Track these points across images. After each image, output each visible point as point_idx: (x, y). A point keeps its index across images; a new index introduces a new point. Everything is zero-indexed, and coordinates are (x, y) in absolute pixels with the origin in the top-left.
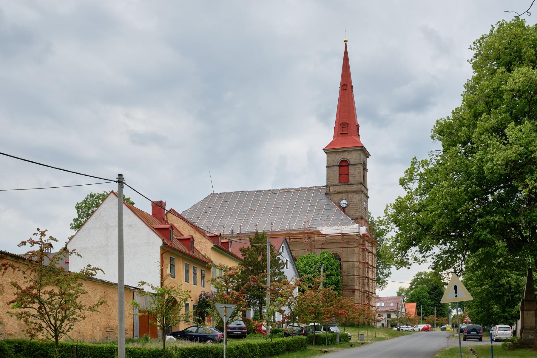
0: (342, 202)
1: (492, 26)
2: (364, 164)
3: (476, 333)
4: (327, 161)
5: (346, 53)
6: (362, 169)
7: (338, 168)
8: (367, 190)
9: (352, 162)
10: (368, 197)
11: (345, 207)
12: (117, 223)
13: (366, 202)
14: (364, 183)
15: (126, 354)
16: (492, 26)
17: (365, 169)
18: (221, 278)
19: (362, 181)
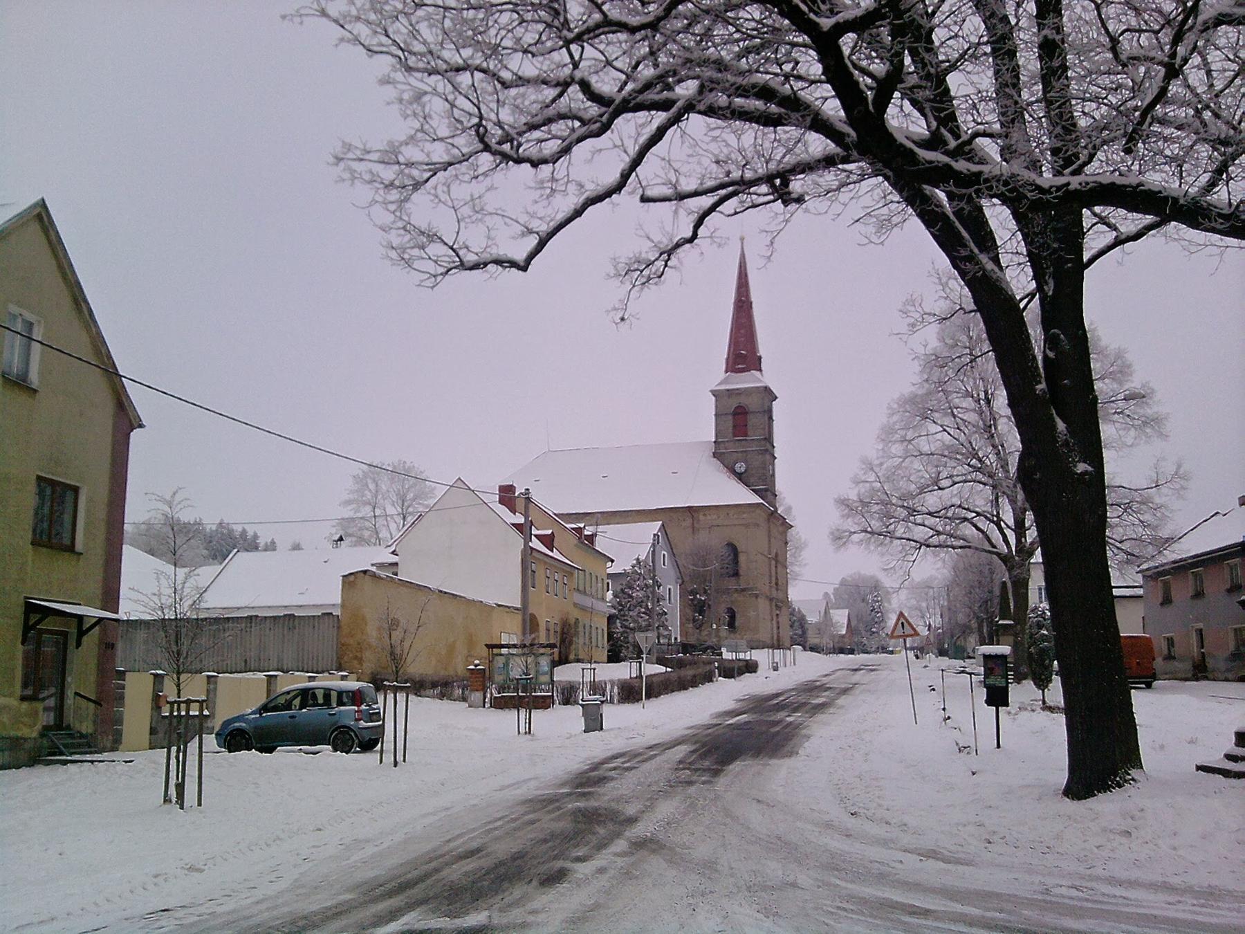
0: (738, 465)
1: (913, 359)
2: (769, 412)
3: (940, 224)
4: (716, 407)
5: (743, 256)
6: (766, 418)
7: (730, 417)
8: (774, 447)
9: (752, 408)
10: (775, 458)
11: (742, 473)
12: (203, 785)
13: (773, 464)
14: (769, 439)
15: (35, 206)
16: (913, 359)
17: (771, 418)
18: (461, 181)
19: (767, 436)
